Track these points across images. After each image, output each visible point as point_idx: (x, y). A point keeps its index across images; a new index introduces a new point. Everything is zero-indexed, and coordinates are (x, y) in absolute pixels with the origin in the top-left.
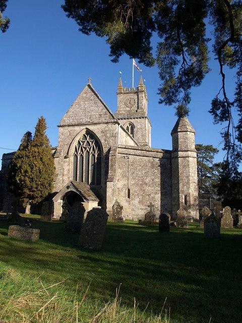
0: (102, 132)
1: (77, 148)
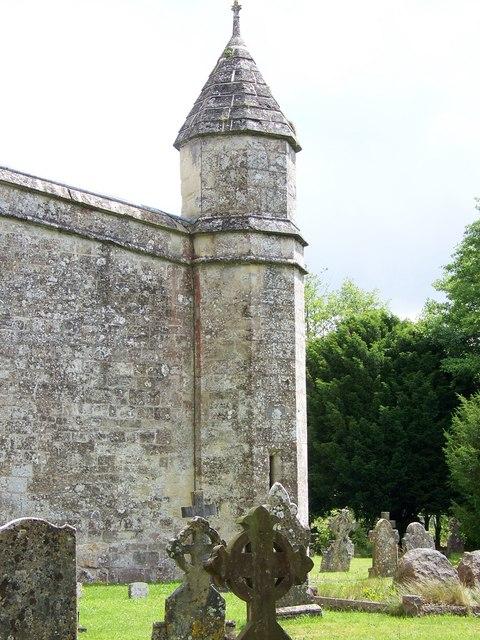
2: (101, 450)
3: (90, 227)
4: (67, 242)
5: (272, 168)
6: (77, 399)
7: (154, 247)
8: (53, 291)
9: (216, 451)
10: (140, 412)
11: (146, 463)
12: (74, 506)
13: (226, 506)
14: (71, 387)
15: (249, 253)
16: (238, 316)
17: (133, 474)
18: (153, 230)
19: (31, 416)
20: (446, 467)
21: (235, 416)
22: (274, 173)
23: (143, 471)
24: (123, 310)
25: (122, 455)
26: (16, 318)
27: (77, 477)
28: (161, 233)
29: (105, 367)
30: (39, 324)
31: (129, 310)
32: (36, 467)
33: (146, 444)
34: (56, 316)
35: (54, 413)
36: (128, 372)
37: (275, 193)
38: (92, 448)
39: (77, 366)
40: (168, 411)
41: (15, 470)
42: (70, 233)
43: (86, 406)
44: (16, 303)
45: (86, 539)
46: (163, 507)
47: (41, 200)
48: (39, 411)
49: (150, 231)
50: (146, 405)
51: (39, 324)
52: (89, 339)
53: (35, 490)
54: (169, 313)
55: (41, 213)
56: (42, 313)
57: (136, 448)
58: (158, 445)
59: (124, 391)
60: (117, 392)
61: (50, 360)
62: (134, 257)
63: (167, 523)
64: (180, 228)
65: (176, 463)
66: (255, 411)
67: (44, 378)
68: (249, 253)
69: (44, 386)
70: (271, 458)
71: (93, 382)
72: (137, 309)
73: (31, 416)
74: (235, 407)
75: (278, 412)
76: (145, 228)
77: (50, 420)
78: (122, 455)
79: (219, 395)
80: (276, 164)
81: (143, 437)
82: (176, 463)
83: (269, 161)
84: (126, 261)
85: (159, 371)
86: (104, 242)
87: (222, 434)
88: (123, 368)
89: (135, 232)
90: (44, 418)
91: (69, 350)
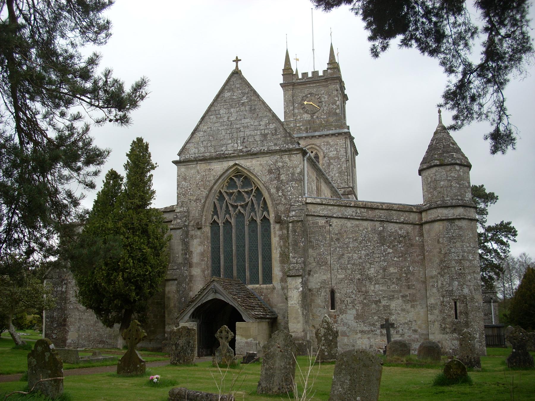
0: (270, 172)
1: (218, 205)
2: (384, 303)
3: (375, 216)
4: (365, 223)
5: (449, 178)
6: (373, 283)
7: (404, 219)
8: (361, 243)
9: (432, 301)
10: (401, 286)
11: (404, 307)
12: (374, 325)
13: (436, 323)
14: (370, 279)
15: (438, 216)
16: (436, 244)
17: (400, 312)
18: (403, 213)
19: (354, 291)
20: (89, 307)
21: (437, 286)
22: (450, 180)
23: (403, 310)
24: (391, 246)
25: (393, 305)
26: (346, 255)
27: (374, 313)
28: (407, 214)
29: (384, 269)
30: (355, 256)
31: (394, 246)
32: (357, 310)
33: (404, 299)
34: (362, 252)
35: (364, 289)
36: (394, 271)
37: (451, 189)
38: (380, 302)
39: (372, 271)
40: (414, 285)
41: (349, 312)
42: (366, 220)
43: (377, 286)
44: (346, 249)
45: (379, 337)
46: (413, 325)
47: (354, 209)
48: (357, 289)
49: (401, 213)
50: (403, 284)
51: (355, 256)
52: (377, 260)
53: (357, 319)
54: (412, 245)
55: (354, 214)
56: (357, 252)
57: (400, 301)
58: (411, 300)
59: (393, 279)
60: (390, 279)
61: (361, 269)
62: (395, 225)
63: (415, 331)
64: (414, 210)
65: (419, 307)
66: (445, 283)
67: (359, 276)
68: (438, 216)
69: (359, 279)
70: (455, 303)
71: (379, 276)
72: (397, 245)
73: (354, 291)
74: (437, 282)
75: (456, 283)
76: (400, 213)
77: (362, 292)
78: (393, 305)
79: (432, 277)
80: (451, 176)
81: (403, 297)
82: (419, 307)
83: (447, 176)
84: (392, 228)
85: (408, 269)
86: (381, 221)
87: (433, 293)
88: (392, 270)
89: (395, 216)
90: (359, 292)
91: (368, 265)
